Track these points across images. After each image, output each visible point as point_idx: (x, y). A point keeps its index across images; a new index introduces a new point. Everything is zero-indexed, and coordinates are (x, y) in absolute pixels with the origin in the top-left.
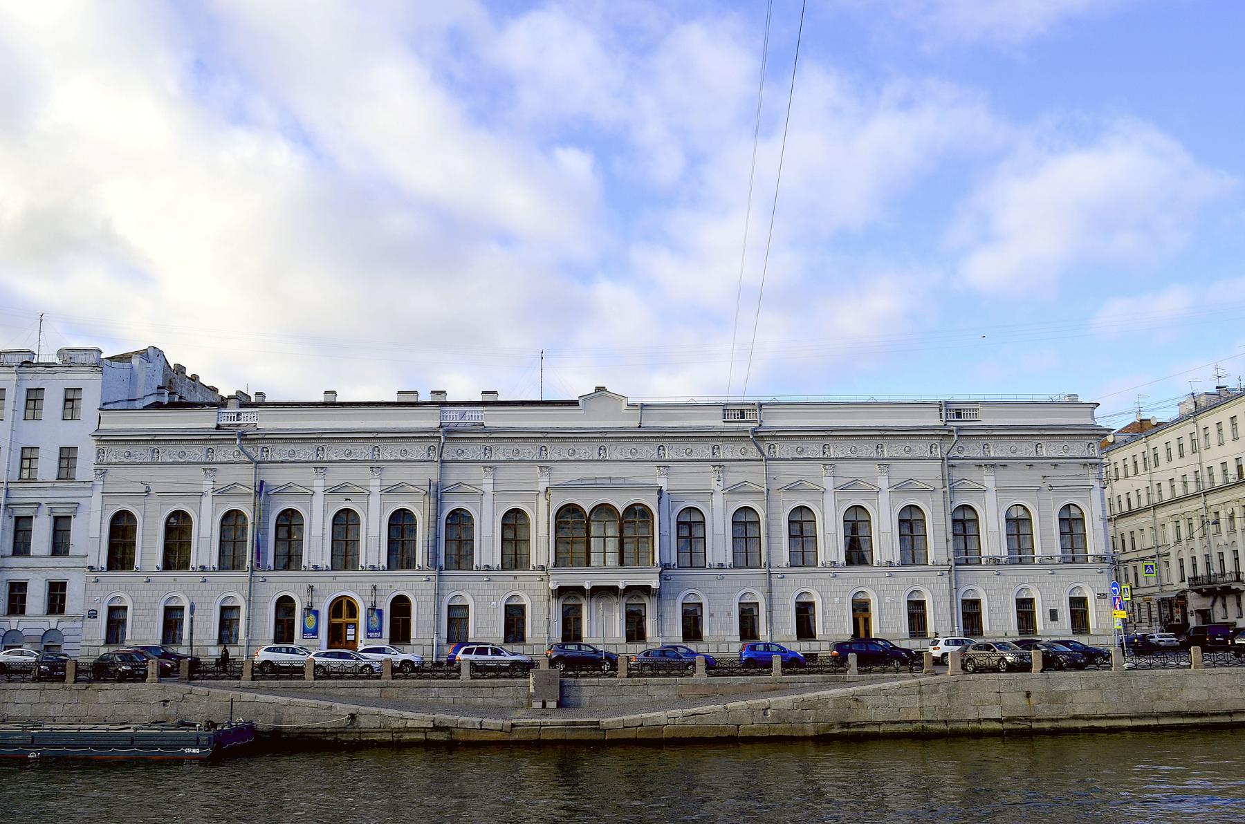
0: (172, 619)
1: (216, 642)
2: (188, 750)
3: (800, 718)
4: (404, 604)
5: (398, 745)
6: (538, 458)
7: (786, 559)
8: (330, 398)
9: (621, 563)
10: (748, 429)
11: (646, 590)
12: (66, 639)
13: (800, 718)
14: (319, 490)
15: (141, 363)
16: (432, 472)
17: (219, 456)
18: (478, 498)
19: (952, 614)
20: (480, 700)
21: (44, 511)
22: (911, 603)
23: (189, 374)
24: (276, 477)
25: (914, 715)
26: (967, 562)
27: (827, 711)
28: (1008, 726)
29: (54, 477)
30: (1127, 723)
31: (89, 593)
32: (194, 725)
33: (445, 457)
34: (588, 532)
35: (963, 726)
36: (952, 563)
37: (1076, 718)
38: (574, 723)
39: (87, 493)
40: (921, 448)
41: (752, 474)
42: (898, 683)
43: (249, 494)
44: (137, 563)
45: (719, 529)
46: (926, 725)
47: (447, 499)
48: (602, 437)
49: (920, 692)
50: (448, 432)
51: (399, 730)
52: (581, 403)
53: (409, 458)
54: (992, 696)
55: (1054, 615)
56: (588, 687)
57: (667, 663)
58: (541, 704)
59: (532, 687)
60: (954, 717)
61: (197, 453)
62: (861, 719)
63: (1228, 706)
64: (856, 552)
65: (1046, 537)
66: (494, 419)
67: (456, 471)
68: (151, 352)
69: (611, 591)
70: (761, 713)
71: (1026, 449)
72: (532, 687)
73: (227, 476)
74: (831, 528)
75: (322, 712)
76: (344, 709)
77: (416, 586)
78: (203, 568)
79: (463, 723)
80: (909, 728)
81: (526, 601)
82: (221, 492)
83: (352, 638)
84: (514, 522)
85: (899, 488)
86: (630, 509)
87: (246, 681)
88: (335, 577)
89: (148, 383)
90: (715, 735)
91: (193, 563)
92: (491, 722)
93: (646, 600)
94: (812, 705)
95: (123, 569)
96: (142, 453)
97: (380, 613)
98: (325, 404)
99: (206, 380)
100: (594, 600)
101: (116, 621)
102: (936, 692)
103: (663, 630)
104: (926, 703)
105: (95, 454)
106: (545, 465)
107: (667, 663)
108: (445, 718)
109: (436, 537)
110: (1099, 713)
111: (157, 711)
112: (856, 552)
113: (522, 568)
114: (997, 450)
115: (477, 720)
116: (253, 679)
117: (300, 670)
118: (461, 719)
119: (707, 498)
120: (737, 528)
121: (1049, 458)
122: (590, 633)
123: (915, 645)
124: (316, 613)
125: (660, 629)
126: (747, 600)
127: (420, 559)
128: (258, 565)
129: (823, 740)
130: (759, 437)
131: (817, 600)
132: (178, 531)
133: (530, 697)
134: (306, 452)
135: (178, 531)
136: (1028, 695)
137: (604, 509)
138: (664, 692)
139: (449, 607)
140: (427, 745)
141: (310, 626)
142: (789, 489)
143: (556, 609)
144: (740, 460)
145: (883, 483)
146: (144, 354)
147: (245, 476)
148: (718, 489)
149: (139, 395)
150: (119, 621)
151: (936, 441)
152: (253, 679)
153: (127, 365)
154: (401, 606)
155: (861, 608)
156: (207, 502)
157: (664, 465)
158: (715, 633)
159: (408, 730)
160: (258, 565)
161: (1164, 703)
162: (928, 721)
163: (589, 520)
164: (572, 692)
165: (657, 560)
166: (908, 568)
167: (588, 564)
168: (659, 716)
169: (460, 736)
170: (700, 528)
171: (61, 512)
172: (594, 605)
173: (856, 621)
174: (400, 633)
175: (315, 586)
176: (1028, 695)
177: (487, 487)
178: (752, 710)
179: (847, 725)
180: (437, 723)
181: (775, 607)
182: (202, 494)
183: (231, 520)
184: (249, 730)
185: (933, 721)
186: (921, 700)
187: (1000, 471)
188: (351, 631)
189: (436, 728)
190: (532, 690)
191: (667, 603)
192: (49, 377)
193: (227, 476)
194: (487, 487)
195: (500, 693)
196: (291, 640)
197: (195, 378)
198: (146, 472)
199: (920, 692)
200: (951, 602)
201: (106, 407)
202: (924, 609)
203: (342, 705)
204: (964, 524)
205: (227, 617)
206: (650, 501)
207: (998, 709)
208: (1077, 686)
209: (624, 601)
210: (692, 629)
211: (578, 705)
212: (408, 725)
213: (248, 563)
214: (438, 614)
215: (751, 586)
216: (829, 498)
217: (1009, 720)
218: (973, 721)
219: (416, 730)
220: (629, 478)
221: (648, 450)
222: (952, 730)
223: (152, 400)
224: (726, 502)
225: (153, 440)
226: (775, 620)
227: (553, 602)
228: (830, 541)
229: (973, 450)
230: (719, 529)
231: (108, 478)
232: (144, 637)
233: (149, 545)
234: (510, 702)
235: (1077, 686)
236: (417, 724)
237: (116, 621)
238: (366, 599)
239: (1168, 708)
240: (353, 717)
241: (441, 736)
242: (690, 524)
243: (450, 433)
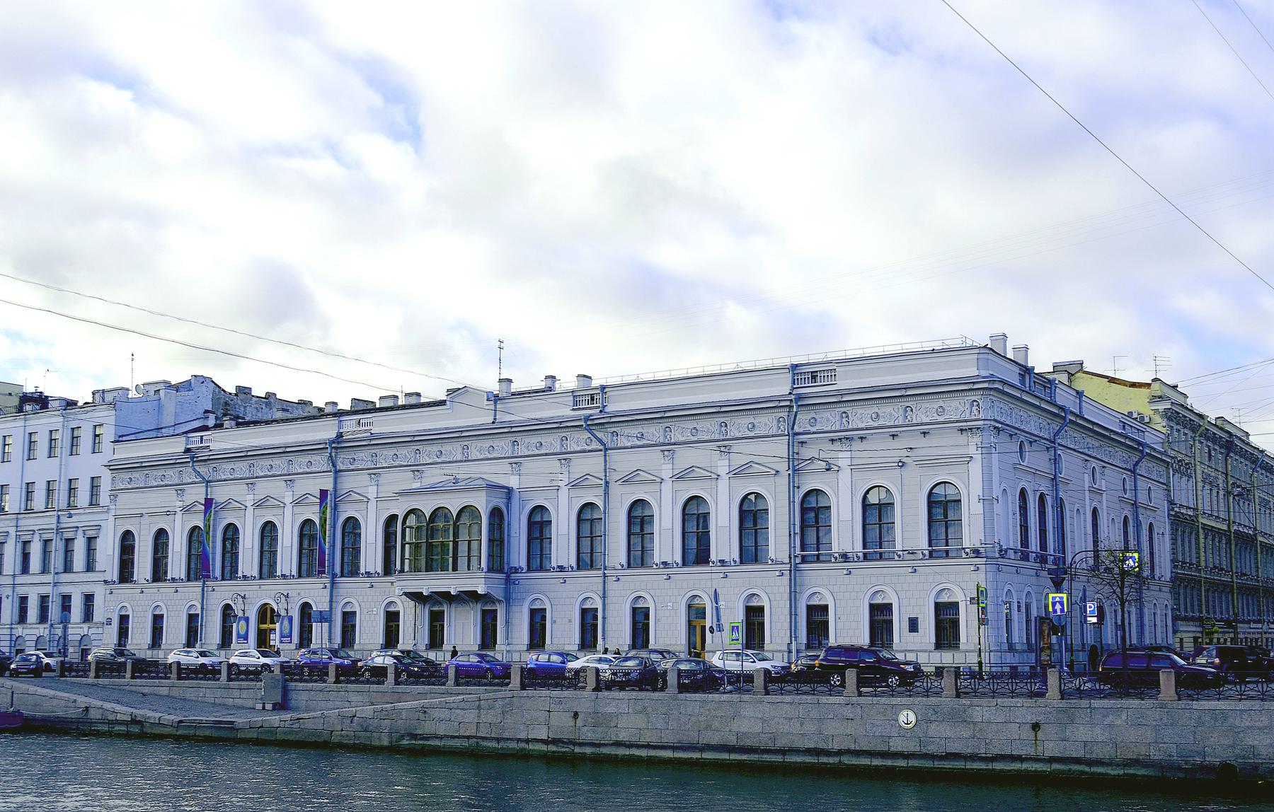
0: (880, 616)
6: (510, 454)
12: (94, 643)
21: (80, 532)
22: (873, 608)
24: (220, 494)
26: (818, 559)
28: (552, 748)
29: (86, 504)
30: (668, 754)
35: (513, 745)
37: (618, 744)
38: (220, 722)
39: (104, 516)
41: (592, 465)
43: (313, 504)
47: (342, 507)
49: (479, 707)
53: (314, 469)
55: (913, 625)
56: (302, 692)
57: (485, 674)
60: (506, 735)
62: (427, 731)
63: (782, 743)
65: (910, 528)
66: (382, 425)
71: (891, 414)
77: (769, 587)
82: (737, 473)
90: (314, 739)
91: (713, 557)
100: (453, 606)
104: (483, 719)
107: (485, 674)
110: (643, 741)
112: (697, 551)
113: (762, 563)
114: (861, 417)
119: (553, 494)
121: (917, 425)
123: (947, 658)
132: (695, 517)
136: (576, 715)
141: (242, 632)
142: (626, 481)
144: (584, 451)
148: (178, 510)
149: (168, 419)
157: (516, 461)
161: (710, 733)
171: (91, 533)
176: (576, 715)
179: (414, 736)
187: (857, 445)
188: (272, 636)
191: (515, 609)
192: (83, 417)
195: (245, 694)
197: (269, 395)
204: (812, 514)
206: (482, 503)
207: (545, 728)
208: (624, 708)
214: (793, 614)
215: (585, 588)
217: (555, 741)
220: (456, 482)
223: (197, 424)
228: (667, 537)
229: (829, 420)
235: (624, 708)
239: (715, 739)
241: (135, 729)
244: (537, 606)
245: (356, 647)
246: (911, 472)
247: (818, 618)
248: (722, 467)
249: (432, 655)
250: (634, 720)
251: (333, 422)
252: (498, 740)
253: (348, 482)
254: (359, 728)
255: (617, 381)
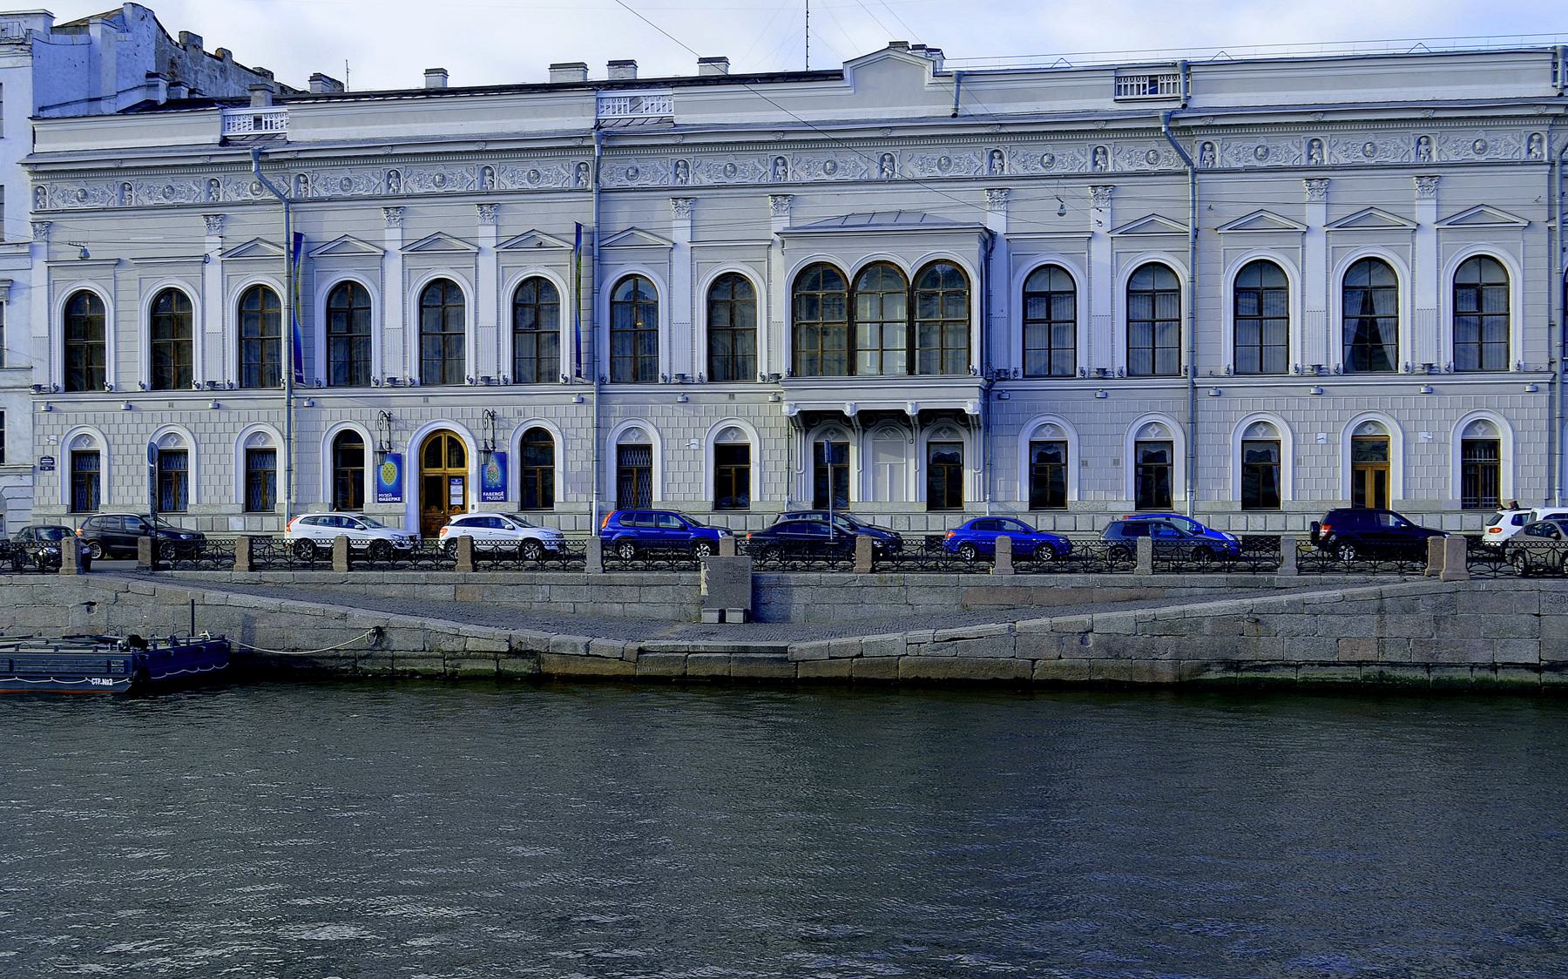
0: (168, 471)
1: (240, 509)
2: (96, 681)
3: (1148, 651)
4: (542, 443)
5: (452, 680)
6: (769, 179)
7: (1227, 359)
8: (436, 82)
9: (911, 369)
10: (1170, 114)
11: (959, 415)
12: (11, 504)
13: (1148, 651)
14: (394, 247)
15: (104, 33)
16: (585, 211)
17: (228, 194)
18: (470, 262)
19: (1551, 466)
20: (618, 607)
22: (1468, 446)
23: (210, 47)
24: (327, 226)
25: (1368, 652)
27: (1198, 640)
31: (39, 430)
32: (114, 642)
33: (606, 182)
34: (852, 313)
36: (1557, 368)
38: (745, 649)
40: (1508, 143)
41: (1169, 201)
42: (1338, 593)
43: (278, 258)
44: (110, 379)
45: (1101, 304)
46: (1388, 671)
47: (611, 259)
48: (886, 137)
49: (1380, 610)
50: (609, 136)
51: (453, 655)
52: (847, 75)
53: (544, 186)
54: (1525, 622)
58: (716, 615)
59: (704, 586)
60: (1445, 657)
61: (192, 189)
62: (1263, 655)
64: (1368, 347)
67: (626, 208)
68: (128, 12)
69: (894, 420)
70: (1076, 640)
72: (704, 586)
73: (243, 227)
74: (1316, 301)
75: (331, 623)
76: (366, 619)
78: (213, 385)
79: (558, 645)
80: (1356, 674)
81: (752, 439)
83: (459, 501)
84: (728, 296)
85: (1457, 223)
86: (928, 272)
87: (240, 572)
88: (171, 403)
89: (123, 70)
90: (991, 675)
91: (197, 377)
92: (604, 645)
93: (964, 436)
94: (1171, 628)
95: (91, 387)
96: (105, 192)
97: (503, 459)
98: (427, 93)
99: (246, 57)
100: (870, 435)
101: (84, 470)
102: (1411, 610)
103: (996, 489)
104: (1392, 630)
105: (30, 196)
106: (783, 193)
108: (529, 636)
109: (594, 327)
111: (77, 621)
112: (1368, 347)
113: (359, 385)
115: (581, 640)
116: (253, 568)
117: (327, 554)
118: (555, 638)
120: (1460, 292)
122: (863, 497)
123: (1259, 523)
124: (398, 459)
125: (989, 489)
126: (1151, 435)
127: (566, 367)
128: (299, 379)
129: (1190, 691)
130: (1178, 128)
131: (1285, 436)
132: (170, 318)
133: (702, 602)
134: (370, 180)
135: (170, 318)
137: (879, 270)
138: (936, 598)
139: (621, 449)
140: (501, 680)
142: (1240, 227)
143: (803, 447)
145: (1425, 213)
146: (113, 19)
147: (271, 226)
148: (1102, 231)
149: (108, 85)
150: (90, 475)
151: (1542, 130)
152: (253, 568)
153: (81, 38)
154: (537, 445)
155: (1369, 454)
156: (213, 272)
157: (1001, 188)
158: (1090, 495)
159: (468, 655)
160: (299, 379)
162: (1393, 664)
163: (852, 290)
164: (773, 597)
165: (976, 362)
166: (1467, 377)
167: (852, 370)
168: (892, 641)
169: (553, 667)
170: (1068, 302)
172: (869, 444)
173: (1358, 479)
174: (537, 494)
175: (393, 414)
177: (681, 234)
178: (1059, 634)
179: (1236, 666)
180: (514, 644)
181: (1203, 450)
182: (206, 259)
183: (255, 302)
184: (219, 649)
185: (1401, 665)
186: (1382, 625)
188: (456, 489)
189: (513, 653)
190: (704, 592)
191: (1002, 441)
193: (243, 227)
194: (681, 234)
195: (652, 595)
196: (359, 502)
197: (223, 55)
198: (542, 208)
199: (1380, 610)
200: (1551, 442)
201: (46, 114)
202: (1497, 455)
203: (363, 612)
205: (258, 465)
206: (968, 257)
209: (925, 437)
210: (1048, 487)
211: (785, 619)
212: (469, 647)
213: (284, 376)
214: (600, 461)
215: (1157, 410)
216: (1316, 245)
218: (1482, 667)
219: (482, 655)
220: (939, 213)
221: (972, 160)
222: (1438, 681)
223: (138, 97)
224: (1116, 256)
225: (119, 168)
226: (1202, 473)
227: (798, 438)
228: (1314, 320)
230: (1101, 304)
231: (58, 236)
232: (128, 501)
233: (127, 349)
234: (667, 612)
236: (484, 646)
237: (84, 470)
238: (479, 434)
240: (379, 632)
242: (1048, 297)
243: (608, 139)
244: (1047, 436)
245: (556, 507)
246: (128, 276)
247: (1482, 459)
248: (392, 238)
249: (1044, 522)
250: (1329, 621)
251: (589, 98)
252: (1428, 667)
253: (622, 217)
254: (1102, 653)
255: (1205, 56)
